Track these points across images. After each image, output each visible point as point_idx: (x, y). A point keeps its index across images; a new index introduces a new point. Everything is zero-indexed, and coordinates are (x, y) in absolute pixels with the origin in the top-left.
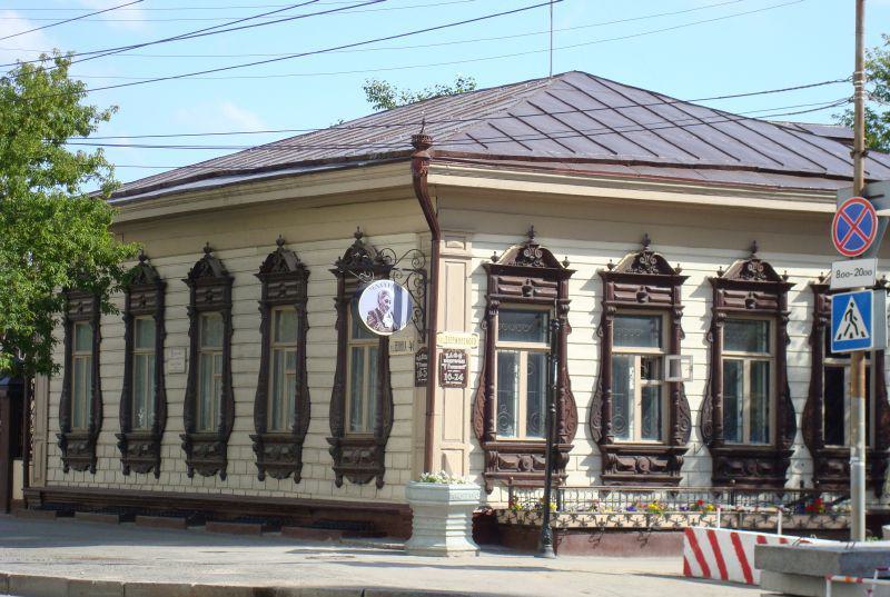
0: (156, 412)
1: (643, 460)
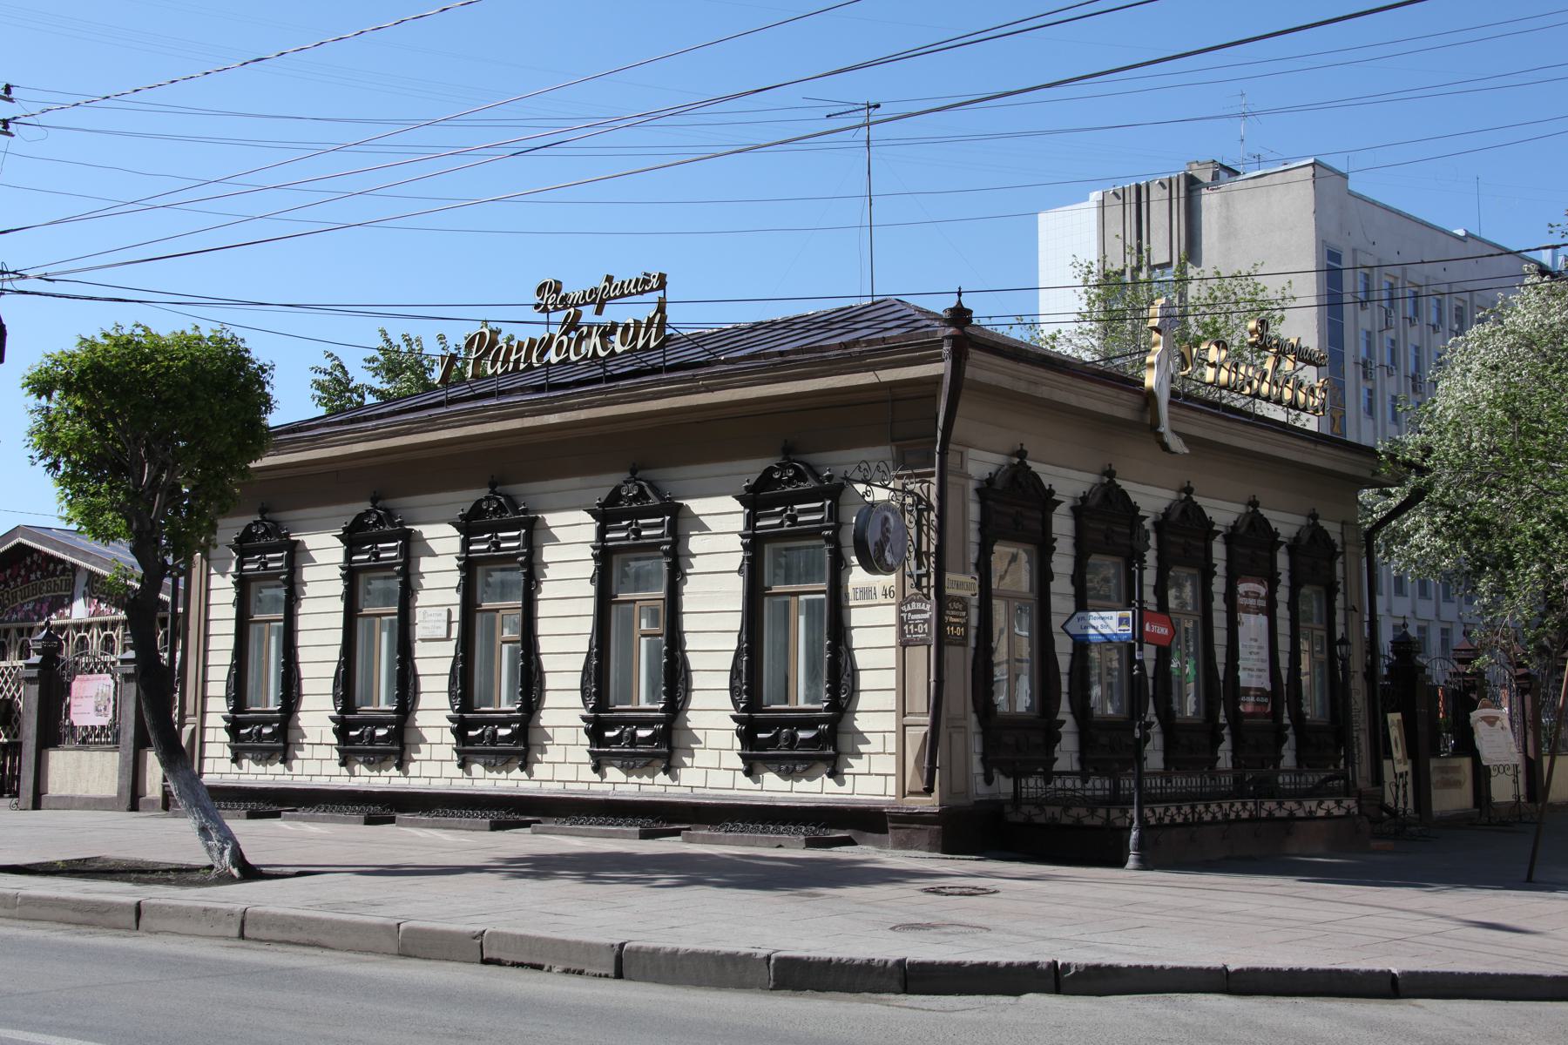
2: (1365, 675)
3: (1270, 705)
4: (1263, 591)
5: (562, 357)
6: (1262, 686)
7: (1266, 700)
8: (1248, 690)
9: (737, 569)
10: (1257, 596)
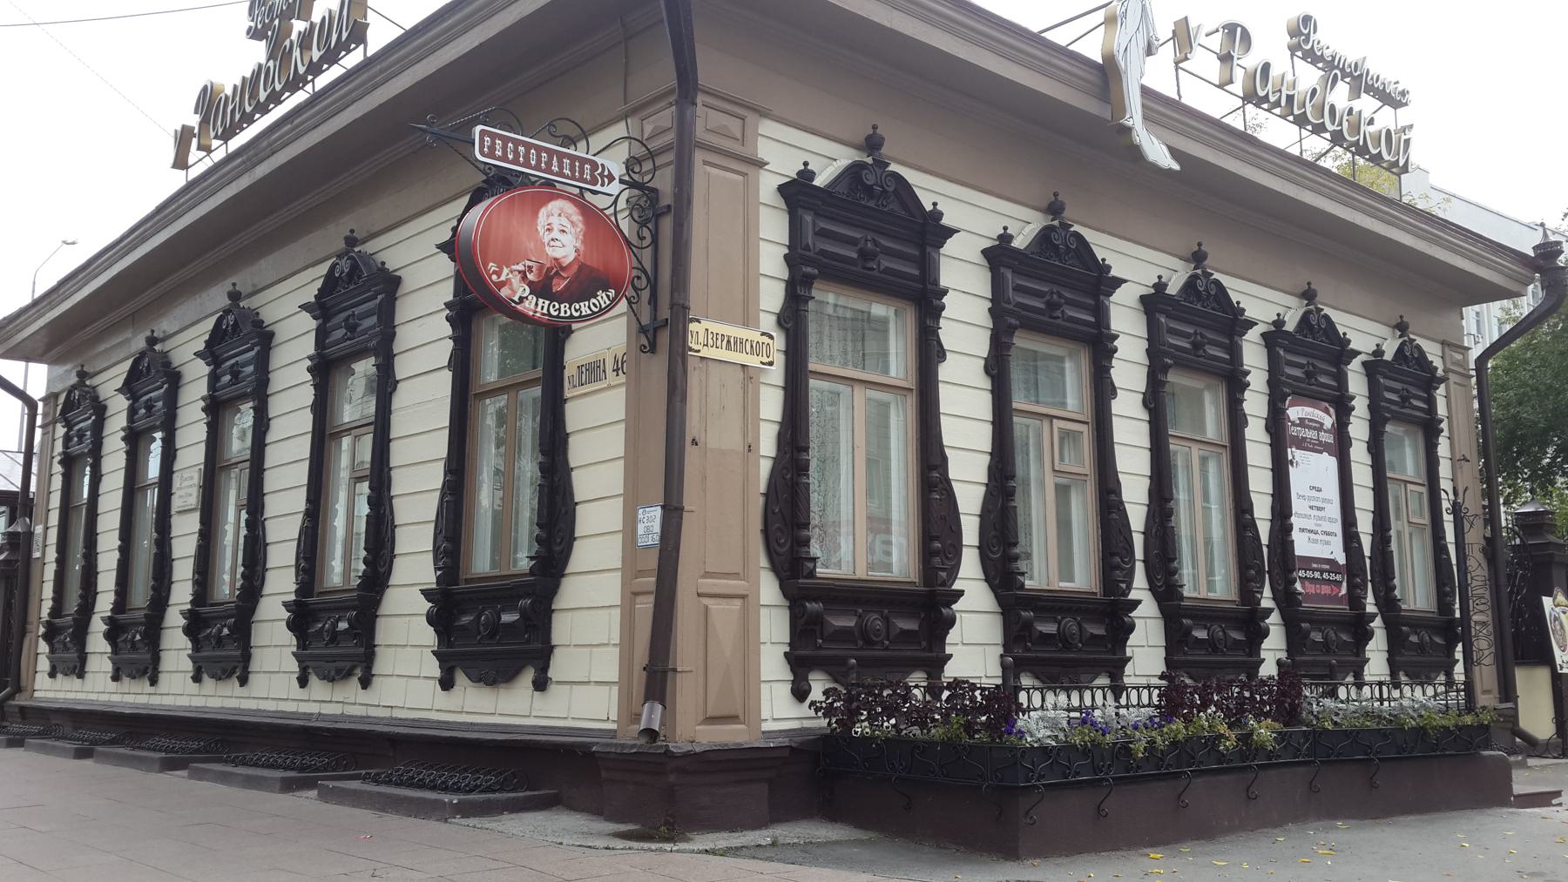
0: (58, 551)
1: (1071, 625)
2: (1484, 551)
3: (1345, 584)
4: (1328, 421)
5: (269, 91)
6: (1331, 557)
7: (1338, 577)
8: (1308, 562)
9: (446, 364)
10: (1320, 427)
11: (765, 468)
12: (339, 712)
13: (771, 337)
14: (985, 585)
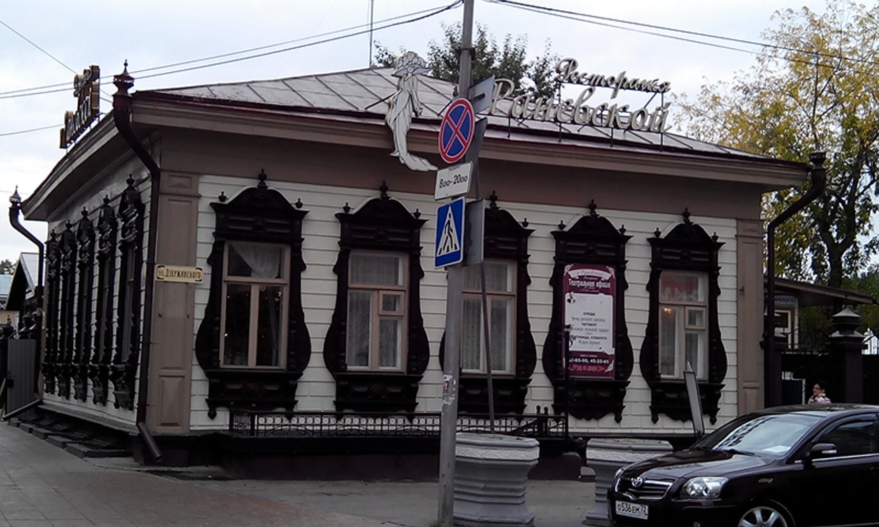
6: (601, 351)
11: (197, 324)
12: (100, 416)
13: (201, 269)
14: (326, 369)
